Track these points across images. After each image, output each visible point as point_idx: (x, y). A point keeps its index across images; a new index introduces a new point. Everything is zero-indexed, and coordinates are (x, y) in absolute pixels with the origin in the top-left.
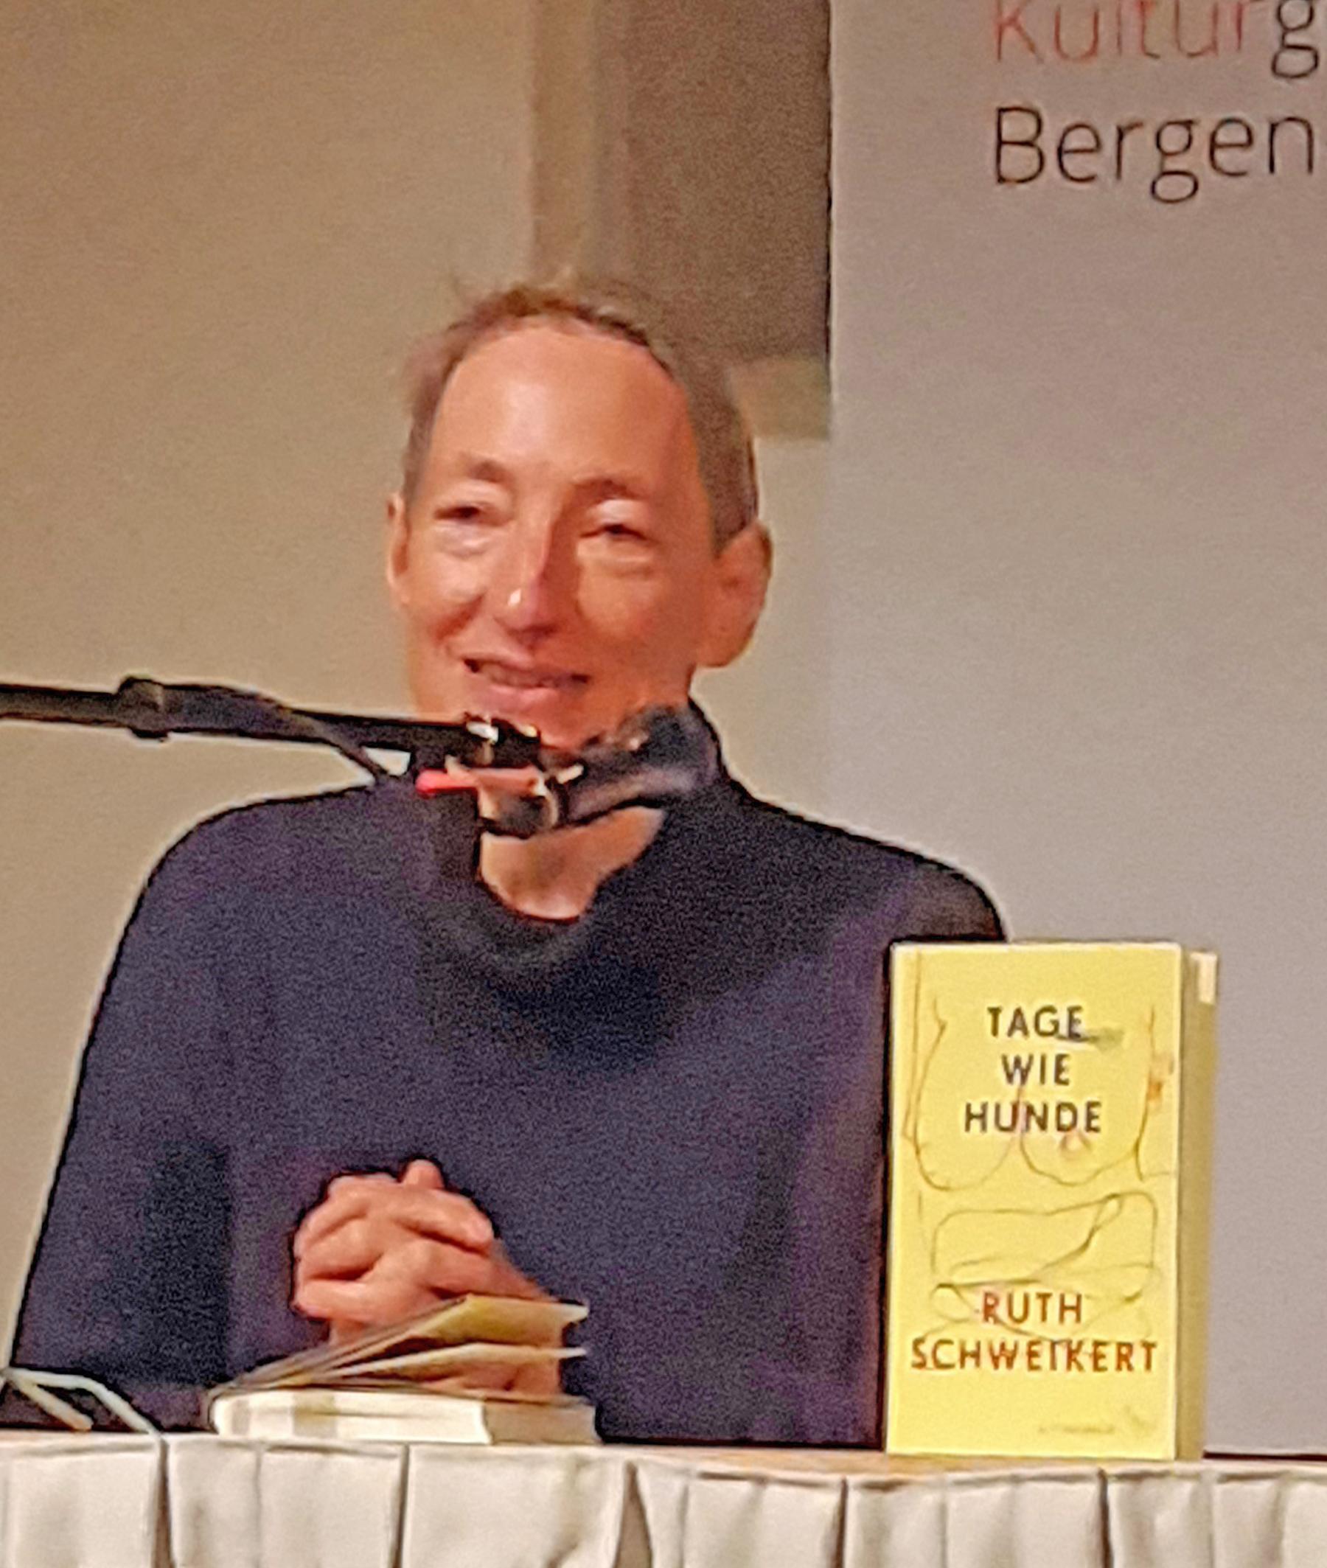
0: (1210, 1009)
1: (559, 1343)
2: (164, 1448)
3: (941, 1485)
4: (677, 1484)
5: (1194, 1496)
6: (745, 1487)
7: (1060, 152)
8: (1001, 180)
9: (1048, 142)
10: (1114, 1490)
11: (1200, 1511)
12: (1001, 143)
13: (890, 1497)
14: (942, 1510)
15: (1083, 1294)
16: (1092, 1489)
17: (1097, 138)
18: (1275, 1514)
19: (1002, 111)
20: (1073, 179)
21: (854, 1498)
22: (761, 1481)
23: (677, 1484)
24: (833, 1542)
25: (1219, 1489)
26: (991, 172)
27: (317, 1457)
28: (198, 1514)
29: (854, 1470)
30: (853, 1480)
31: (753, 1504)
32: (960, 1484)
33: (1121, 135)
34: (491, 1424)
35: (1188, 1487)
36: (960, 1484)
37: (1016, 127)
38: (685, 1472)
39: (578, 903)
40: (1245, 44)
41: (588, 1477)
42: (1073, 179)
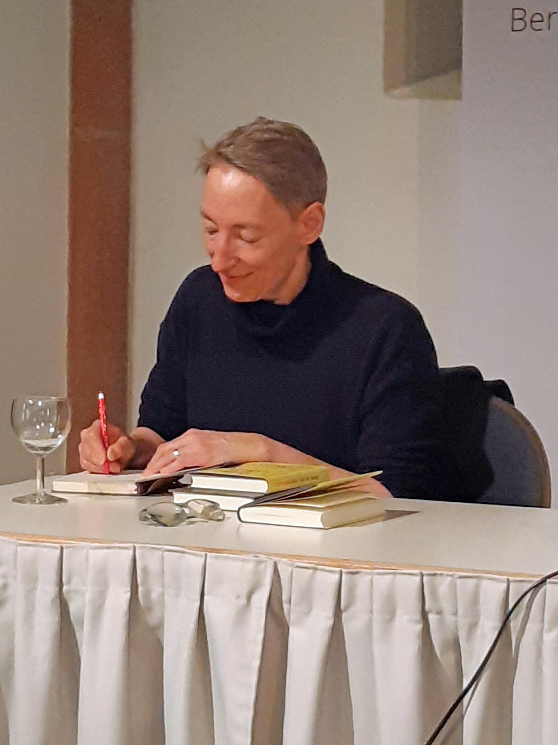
2: (206, 555)
4: (290, 569)
5: (452, 581)
8: (513, 31)
9: (528, 19)
10: (425, 578)
11: (453, 588)
12: (514, 19)
14: (372, 580)
15: (63, 545)
16: (418, 578)
17: (531, 26)
19: (513, 9)
21: (344, 576)
22: (316, 569)
23: (290, 569)
24: (337, 593)
25: (459, 581)
27: (179, 554)
28: (145, 571)
29: (345, 567)
30: (344, 570)
31: (312, 576)
33: (550, 16)
34: (507, 390)
35: (449, 578)
37: (518, 14)
38: (292, 565)
39: (113, 457)
40: (12, 401)
41: (262, 566)
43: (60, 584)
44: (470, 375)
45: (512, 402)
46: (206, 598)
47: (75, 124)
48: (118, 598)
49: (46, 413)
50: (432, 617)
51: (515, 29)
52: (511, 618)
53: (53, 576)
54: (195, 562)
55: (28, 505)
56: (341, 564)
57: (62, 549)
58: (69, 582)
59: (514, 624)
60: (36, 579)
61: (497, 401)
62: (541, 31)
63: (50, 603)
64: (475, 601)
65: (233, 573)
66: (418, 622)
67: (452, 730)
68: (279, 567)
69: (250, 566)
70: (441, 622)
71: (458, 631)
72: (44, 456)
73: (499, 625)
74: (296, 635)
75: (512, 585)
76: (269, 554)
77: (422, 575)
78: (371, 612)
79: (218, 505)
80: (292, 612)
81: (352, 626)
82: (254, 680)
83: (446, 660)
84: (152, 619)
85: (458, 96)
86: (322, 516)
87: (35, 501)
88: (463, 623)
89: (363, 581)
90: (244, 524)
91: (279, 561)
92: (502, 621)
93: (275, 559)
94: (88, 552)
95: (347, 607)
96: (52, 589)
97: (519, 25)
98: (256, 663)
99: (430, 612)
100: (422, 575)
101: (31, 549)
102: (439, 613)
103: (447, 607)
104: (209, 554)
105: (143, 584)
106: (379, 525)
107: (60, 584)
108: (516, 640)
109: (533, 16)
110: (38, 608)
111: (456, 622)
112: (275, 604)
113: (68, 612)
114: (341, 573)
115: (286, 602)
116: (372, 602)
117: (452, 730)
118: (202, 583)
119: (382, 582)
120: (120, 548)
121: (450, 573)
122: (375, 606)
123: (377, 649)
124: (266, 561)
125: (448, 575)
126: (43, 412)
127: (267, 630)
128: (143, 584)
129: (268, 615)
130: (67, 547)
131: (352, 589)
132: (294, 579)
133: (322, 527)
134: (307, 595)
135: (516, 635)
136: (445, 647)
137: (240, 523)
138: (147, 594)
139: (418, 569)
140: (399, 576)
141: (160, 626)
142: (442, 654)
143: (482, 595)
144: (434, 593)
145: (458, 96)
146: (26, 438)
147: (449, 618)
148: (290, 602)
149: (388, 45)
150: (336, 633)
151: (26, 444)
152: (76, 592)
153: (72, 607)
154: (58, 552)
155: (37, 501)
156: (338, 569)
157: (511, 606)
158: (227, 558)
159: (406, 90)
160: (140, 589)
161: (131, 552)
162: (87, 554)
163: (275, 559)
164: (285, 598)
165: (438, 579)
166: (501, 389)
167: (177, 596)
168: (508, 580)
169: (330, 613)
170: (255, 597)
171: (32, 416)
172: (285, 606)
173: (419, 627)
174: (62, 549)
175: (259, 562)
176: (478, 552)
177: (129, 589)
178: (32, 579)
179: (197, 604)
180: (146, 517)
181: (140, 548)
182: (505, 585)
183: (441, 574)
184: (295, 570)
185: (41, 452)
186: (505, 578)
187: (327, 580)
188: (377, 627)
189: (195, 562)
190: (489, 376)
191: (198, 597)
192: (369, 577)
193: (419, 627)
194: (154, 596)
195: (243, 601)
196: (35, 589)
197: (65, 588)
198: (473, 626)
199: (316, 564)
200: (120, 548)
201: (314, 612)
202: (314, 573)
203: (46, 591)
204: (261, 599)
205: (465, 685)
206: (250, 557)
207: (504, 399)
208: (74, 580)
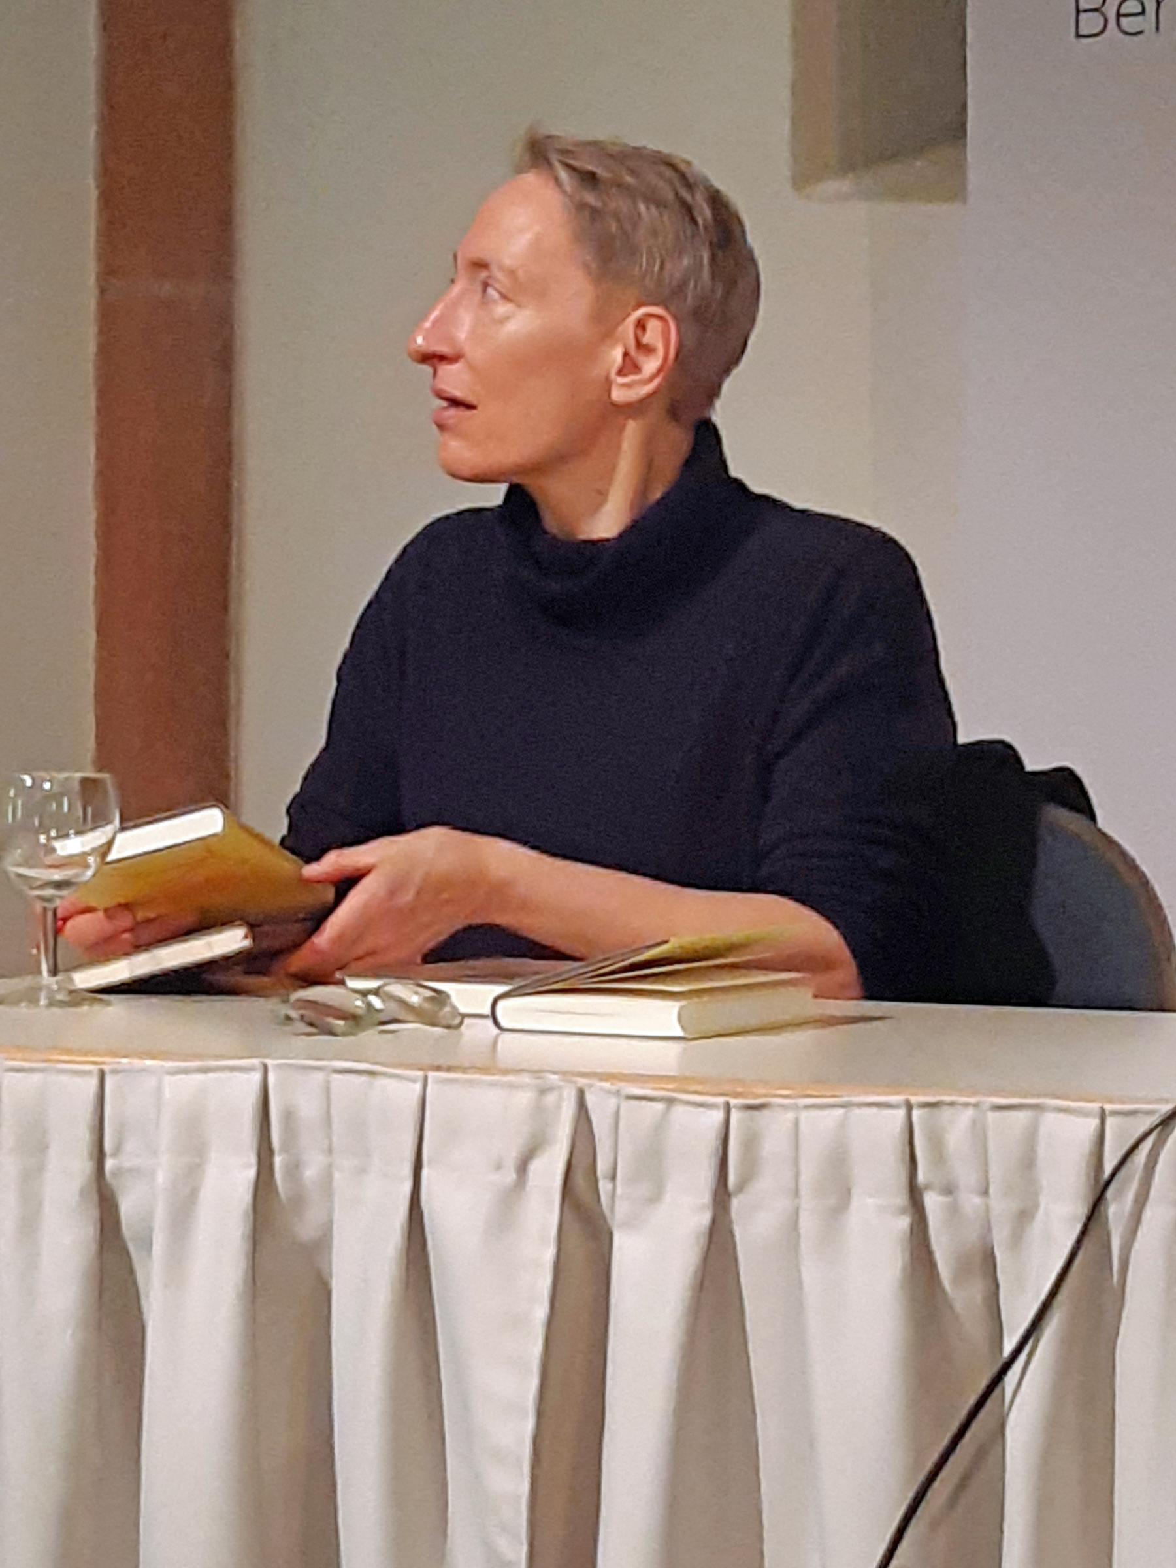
0: (253, 927)
1: (857, 990)
2: (426, 1079)
3: (796, 1107)
4: (613, 1101)
5: (974, 1122)
6: (659, 1106)
7: (1119, 15)
10: (916, 1114)
11: (979, 1133)
12: (1078, 11)
13: (935, 1111)
14: (797, 1124)
15: (106, 1068)
16: (902, 1112)
18: (1031, 1137)
20: (1126, 33)
21: (735, 1116)
22: (670, 1101)
25: (991, 1116)
26: (1140, 18)
28: (289, 1116)
29: (737, 1095)
32: (807, 1107)
35: (970, 1112)
36: (807, 1107)
38: (618, 1093)
41: (551, 1098)
42: (1126, 33)
43: (100, 1156)
44: (999, 756)
45: (1093, 817)
46: (425, 1172)
47: (108, 272)
48: (230, 1178)
49: (60, 805)
50: (932, 1201)
51: (1081, 32)
52: (1110, 1193)
53: (83, 1136)
54: (400, 1092)
55: (23, 1009)
56: (727, 1088)
57: (102, 1076)
58: (118, 1149)
59: (1117, 1210)
60: (42, 1148)
61: (1059, 816)
62: (1141, 36)
63: (77, 1198)
64: (1028, 1162)
65: (481, 1122)
66: (903, 1211)
67: (981, 1454)
68: (590, 1099)
69: (524, 1099)
70: (954, 1210)
71: (989, 1229)
72: (58, 902)
73: (1082, 1211)
74: (628, 1251)
75: (1110, 1121)
76: (566, 1074)
77: (909, 1107)
78: (797, 1193)
79: (448, 996)
80: (619, 1200)
81: (754, 1226)
82: (536, 1349)
83: (964, 1297)
84: (306, 1230)
85: (956, 191)
86: (682, 1008)
87: (38, 1000)
88: (1001, 1207)
89: (775, 1128)
90: (507, 1036)
91: (591, 1086)
92: (1091, 1201)
93: (582, 1081)
94: (160, 1081)
95: (741, 1188)
96: (81, 1167)
97: (1090, 23)
98: (541, 1312)
99: (928, 1187)
100: (909, 1107)
101: (36, 1077)
102: (949, 1190)
103: (966, 1176)
104: (432, 1075)
105: (285, 1149)
106: (804, 1038)
107: (100, 1156)
108: (1122, 1249)
109: (1120, 6)
110: (47, 1209)
111: (988, 1209)
112: (580, 1180)
113: (118, 1223)
114: (728, 1108)
115: (605, 1178)
116: (797, 1175)
117: (981, 1454)
118: (416, 1141)
119: (819, 1124)
120: (233, 1069)
121: (973, 1100)
122: (804, 1178)
123: (811, 1274)
124: (560, 1088)
125: (966, 1105)
126: (54, 805)
127: (557, 1305)
128: (285, 1149)
129: (566, 1209)
130: (115, 1072)
131: (751, 1143)
132: (622, 1129)
133: (680, 1033)
134: (653, 1162)
135: (1121, 1229)
136: (962, 1271)
137: (496, 1031)
138: (295, 1168)
139: (898, 1093)
140: (857, 1111)
141: (322, 1244)
142: (956, 1280)
143: (1042, 1150)
144: (937, 1144)
145: (956, 191)
146: (19, 865)
147: (971, 1202)
148: (613, 1178)
149: (802, 89)
150: (718, 1241)
151: (19, 876)
152: (135, 1171)
153: (127, 1207)
154: (94, 1081)
155: (43, 1002)
156: (720, 1100)
157: (1108, 1169)
158: (471, 1082)
159: (843, 185)
160: (278, 1160)
161: (257, 1077)
162: (159, 1090)
163: (582, 1081)
164: (602, 1166)
165: (946, 1113)
166: (1066, 788)
167: (362, 1171)
168: (1103, 1111)
169: (702, 1193)
170: (536, 1167)
171: (28, 816)
172: (604, 1186)
173: (904, 1222)
174: (102, 1076)
175: (543, 1091)
176: (1030, 1108)
177: (253, 1160)
178: (35, 1144)
179: (407, 1186)
180: (288, 1018)
181: (279, 1066)
182: (1094, 1122)
183: (952, 1104)
184: (626, 1105)
185: (49, 892)
186: (1095, 1106)
187: (697, 1125)
188: (808, 1224)
189: (400, 1092)
190: (1036, 760)
191: (407, 1170)
192: (790, 1115)
193: (904, 1222)
194: (310, 1173)
195: (511, 1176)
196: (41, 1168)
197: (109, 1164)
198: (1024, 1216)
199: (670, 1090)
200: (233, 1069)
201: (668, 1197)
202: (668, 1110)
203: (67, 1173)
204: (549, 1169)
205: (1008, 1347)
206: (526, 1079)
207: (1073, 808)
208: (130, 1146)
